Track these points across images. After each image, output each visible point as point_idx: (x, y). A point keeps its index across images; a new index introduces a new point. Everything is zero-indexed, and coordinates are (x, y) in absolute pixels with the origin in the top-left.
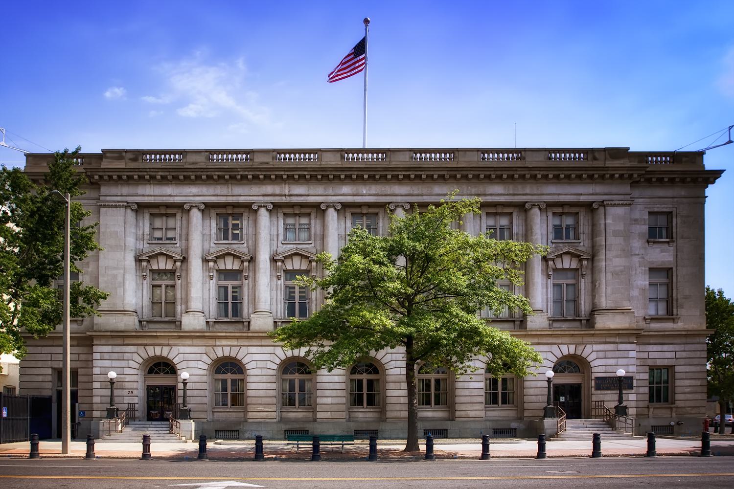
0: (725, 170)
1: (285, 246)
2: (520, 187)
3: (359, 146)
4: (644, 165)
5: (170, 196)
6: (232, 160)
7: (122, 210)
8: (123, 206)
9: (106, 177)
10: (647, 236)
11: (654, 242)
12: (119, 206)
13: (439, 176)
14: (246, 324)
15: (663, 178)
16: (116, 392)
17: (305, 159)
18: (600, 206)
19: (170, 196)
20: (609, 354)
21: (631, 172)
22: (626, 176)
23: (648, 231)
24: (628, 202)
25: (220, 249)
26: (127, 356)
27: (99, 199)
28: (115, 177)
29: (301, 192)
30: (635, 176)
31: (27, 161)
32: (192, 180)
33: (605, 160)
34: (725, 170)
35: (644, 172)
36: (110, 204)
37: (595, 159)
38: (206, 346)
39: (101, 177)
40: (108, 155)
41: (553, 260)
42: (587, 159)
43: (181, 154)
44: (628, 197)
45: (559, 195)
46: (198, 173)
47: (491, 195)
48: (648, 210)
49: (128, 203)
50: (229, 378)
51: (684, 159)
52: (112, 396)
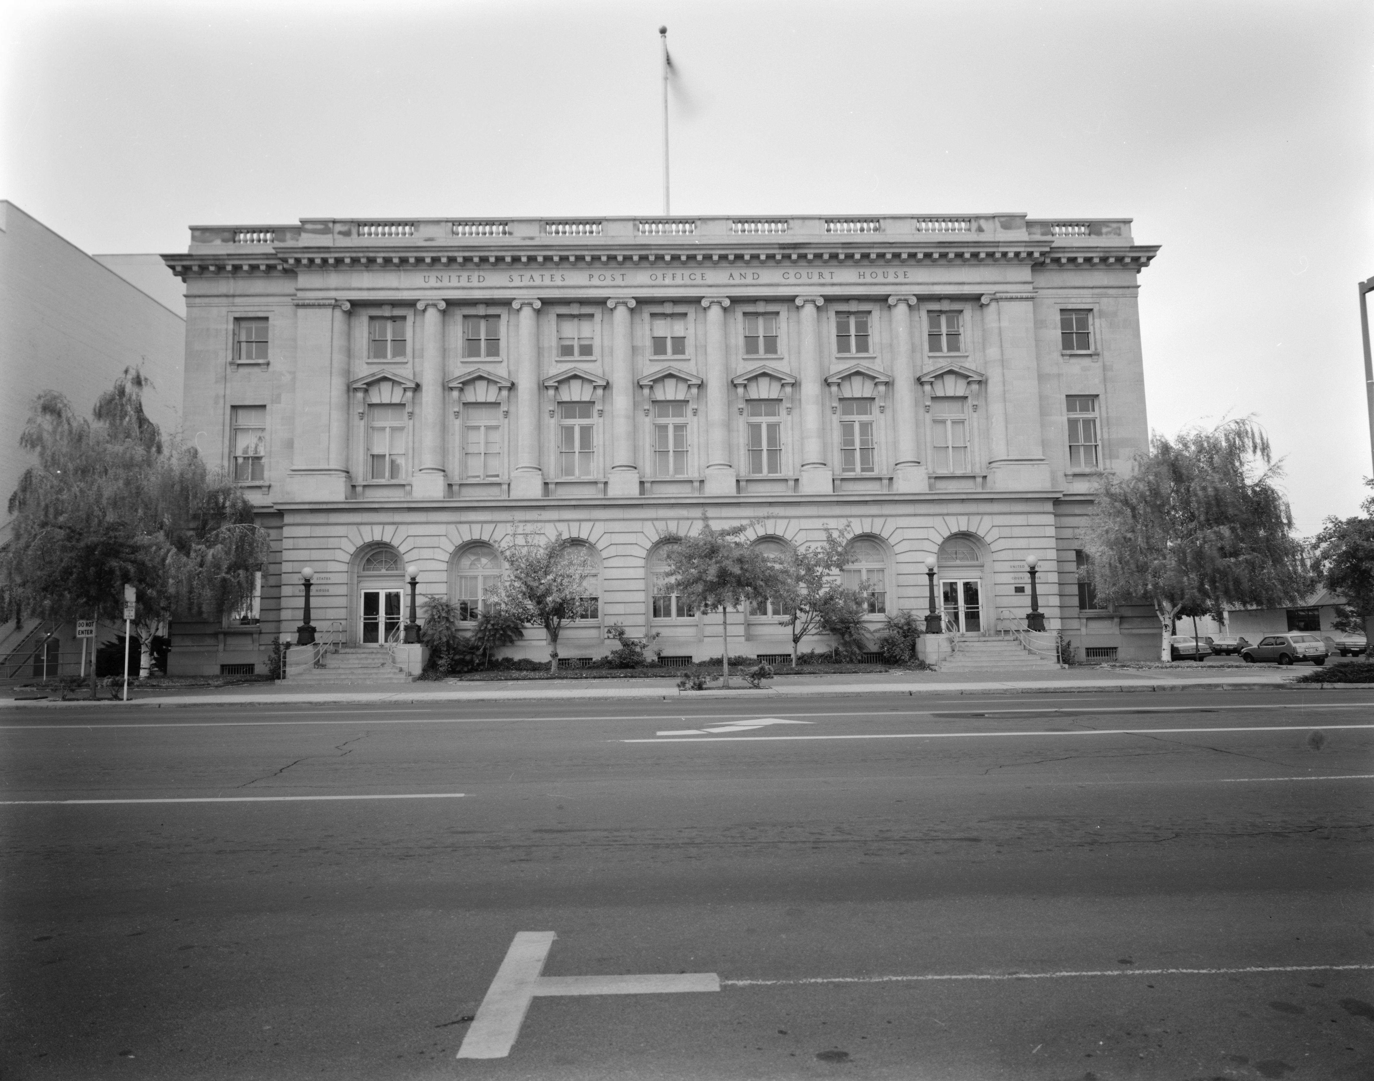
0: (1159, 247)
1: (559, 365)
2: (880, 271)
3: (658, 212)
4: (1049, 238)
5: (397, 289)
6: (763, 231)
7: (329, 311)
8: (330, 305)
9: (305, 261)
10: (1060, 346)
11: (1071, 356)
12: (324, 305)
13: (784, 256)
14: (505, 487)
15: (1139, 258)
16: (314, 602)
17: (684, 232)
18: (992, 300)
19: (397, 289)
20: (1017, 532)
21: (1030, 249)
22: (1023, 255)
23: (1060, 339)
24: (1029, 295)
25: (939, 366)
26: (332, 543)
27: (295, 295)
28: (318, 261)
29: (576, 282)
30: (1036, 255)
31: (193, 238)
32: (935, 261)
33: (995, 231)
34: (1159, 247)
35: (1048, 249)
36: (1014, 295)
37: (980, 230)
38: (967, 514)
39: (298, 261)
40: (308, 226)
41: (931, 383)
42: (969, 230)
43: (412, 225)
44: (1030, 287)
45: (933, 284)
46: (371, 255)
47: (840, 285)
48: (1059, 307)
49: (336, 300)
50: (480, 574)
51: (1104, 230)
52: (307, 609)
